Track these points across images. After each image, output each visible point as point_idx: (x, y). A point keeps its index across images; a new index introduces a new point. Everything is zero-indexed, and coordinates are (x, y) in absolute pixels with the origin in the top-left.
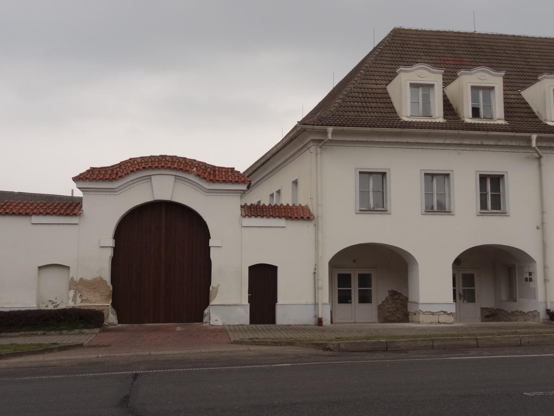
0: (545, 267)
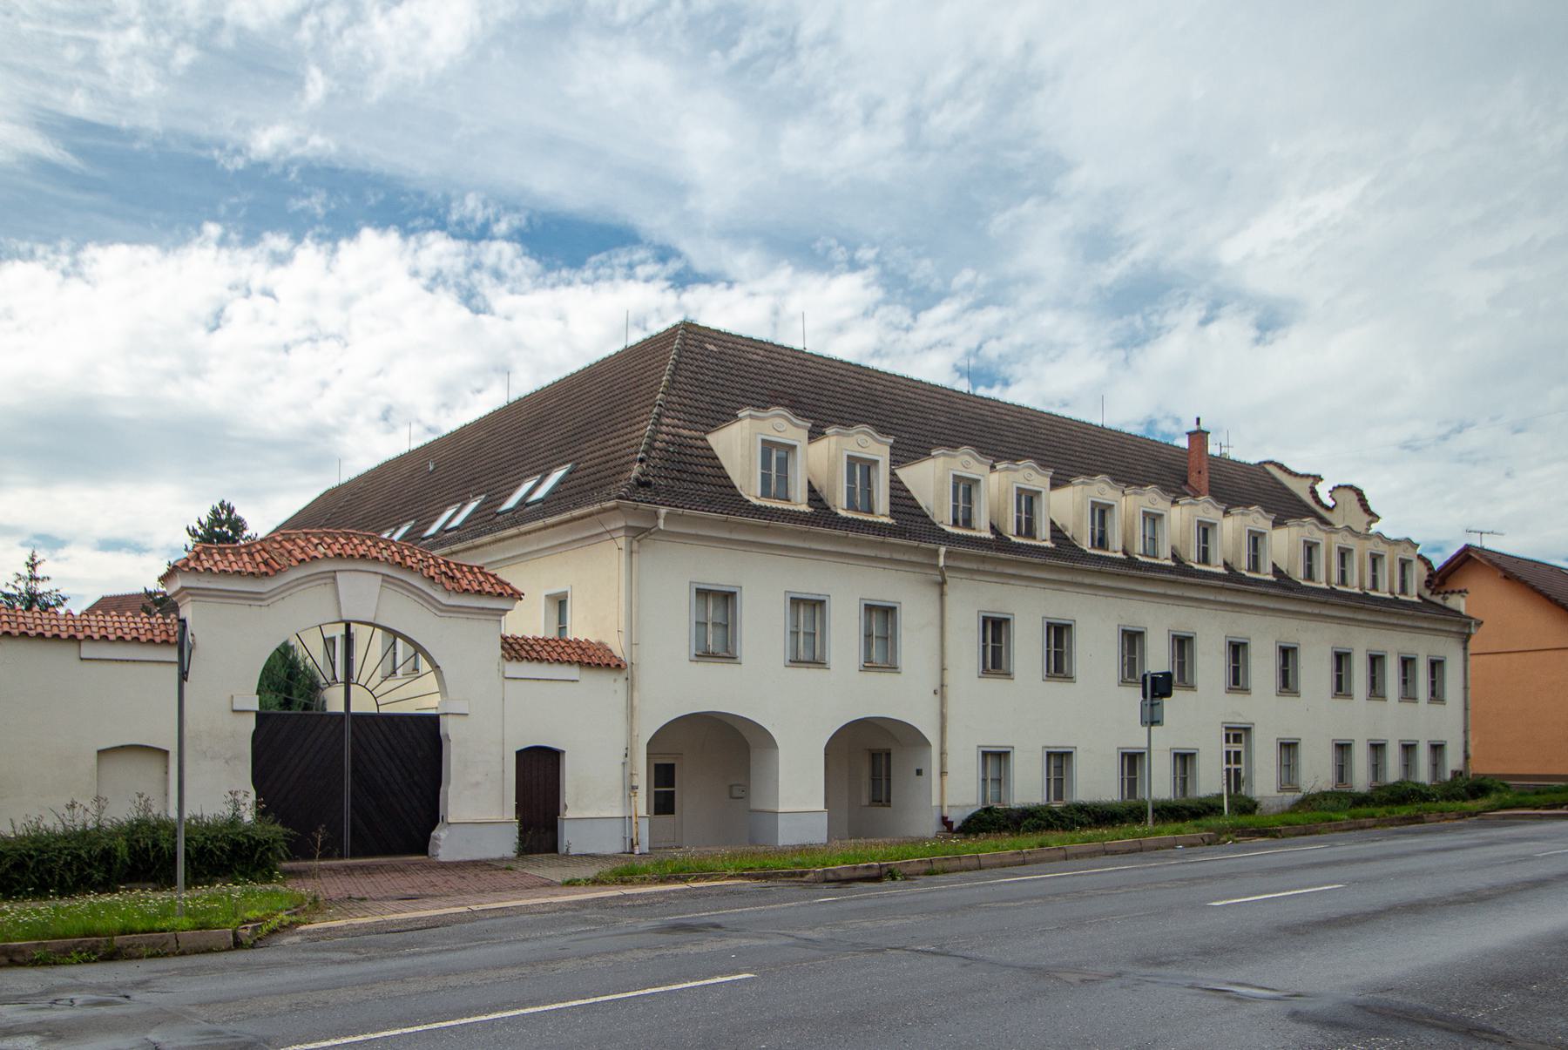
0: (942, 753)
